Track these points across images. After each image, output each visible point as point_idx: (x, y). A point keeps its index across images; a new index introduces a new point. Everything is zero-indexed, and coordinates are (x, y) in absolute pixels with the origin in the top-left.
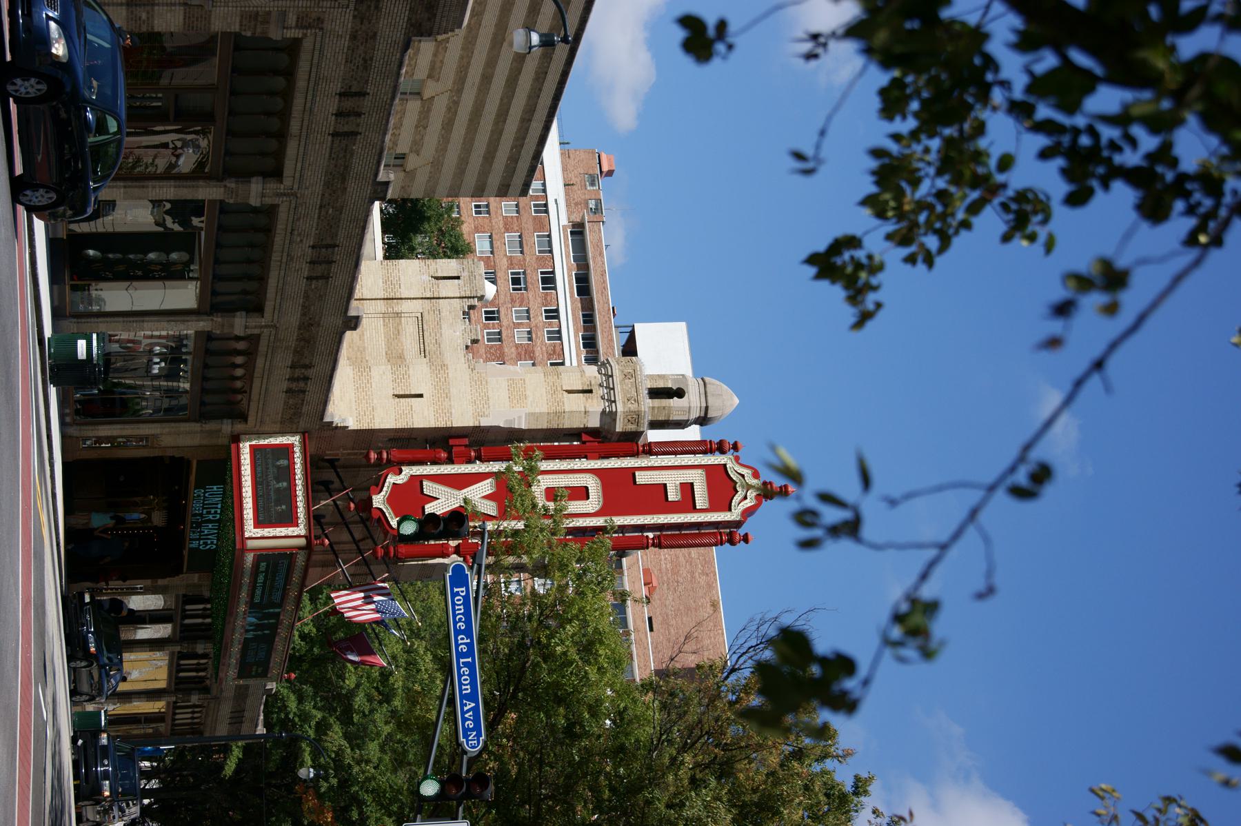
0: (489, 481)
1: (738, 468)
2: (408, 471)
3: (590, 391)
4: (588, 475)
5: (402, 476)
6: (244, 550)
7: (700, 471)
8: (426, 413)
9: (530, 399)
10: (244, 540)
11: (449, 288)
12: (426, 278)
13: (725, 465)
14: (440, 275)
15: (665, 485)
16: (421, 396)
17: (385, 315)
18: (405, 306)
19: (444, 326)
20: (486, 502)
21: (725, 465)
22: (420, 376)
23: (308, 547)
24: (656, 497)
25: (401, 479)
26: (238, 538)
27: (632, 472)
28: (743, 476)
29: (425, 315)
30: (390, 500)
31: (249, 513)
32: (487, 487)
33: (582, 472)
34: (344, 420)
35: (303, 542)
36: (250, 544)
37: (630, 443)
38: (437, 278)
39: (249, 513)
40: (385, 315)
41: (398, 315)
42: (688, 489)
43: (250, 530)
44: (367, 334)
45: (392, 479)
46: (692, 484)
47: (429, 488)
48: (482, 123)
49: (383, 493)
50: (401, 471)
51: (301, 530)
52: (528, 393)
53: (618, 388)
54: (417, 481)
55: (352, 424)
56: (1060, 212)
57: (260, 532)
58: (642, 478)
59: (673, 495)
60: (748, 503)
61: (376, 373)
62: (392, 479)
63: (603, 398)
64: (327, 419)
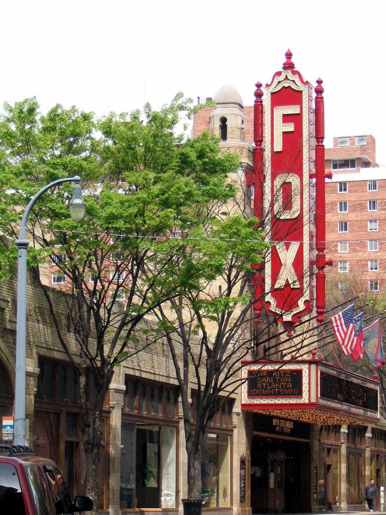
1: (273, 86)
7: (275, 110)
15: (284, 133)
24: (292, 140)
27: (275, 154)
32: (280, 247)
42: (287, 118)
50: (269, 303)
58: (278, 147)
59: (290, 127)
62: (273, 308)
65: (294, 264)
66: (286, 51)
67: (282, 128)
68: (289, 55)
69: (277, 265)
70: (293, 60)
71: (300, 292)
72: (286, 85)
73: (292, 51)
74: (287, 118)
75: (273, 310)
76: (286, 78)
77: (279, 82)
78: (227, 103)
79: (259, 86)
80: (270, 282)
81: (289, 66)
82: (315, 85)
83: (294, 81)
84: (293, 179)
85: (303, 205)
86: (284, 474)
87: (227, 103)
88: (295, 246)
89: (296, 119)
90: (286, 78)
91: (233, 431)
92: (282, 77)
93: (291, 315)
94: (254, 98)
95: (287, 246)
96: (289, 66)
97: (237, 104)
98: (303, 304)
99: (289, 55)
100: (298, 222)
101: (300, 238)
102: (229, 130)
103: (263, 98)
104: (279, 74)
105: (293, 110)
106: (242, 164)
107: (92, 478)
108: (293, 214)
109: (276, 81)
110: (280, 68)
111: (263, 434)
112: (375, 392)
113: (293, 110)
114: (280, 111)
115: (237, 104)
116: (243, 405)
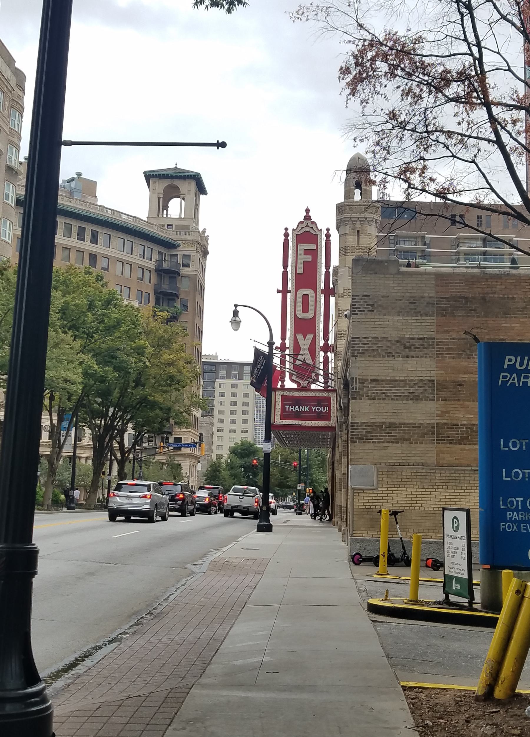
42: (307, 252)
58: (300, 271)
59: (309, 258)
65: (309, 349)
67: (303, 258)
68: (307, 211)
70: (310, 214)
73: (309, 208)
74: (307, 252)
76: (307, 226)
77: (302, 228)
79: (286, 229)
81: (307, 218)
82: (326, 232)
83: (312, 228)
84: (310, 292)
86: (464, 270)
89: (314, 253)
90: (307, 226)
92: (305, 224)
94: (284, 238)
96: (307, 218)
99: (307, 211)
100: (313, 321)
103: (289, 238)
105: (312, 247)
108: (301, 292)
111: (18, 719)
112: (255, 490)
113: (312, 247)
114: (302, 247)
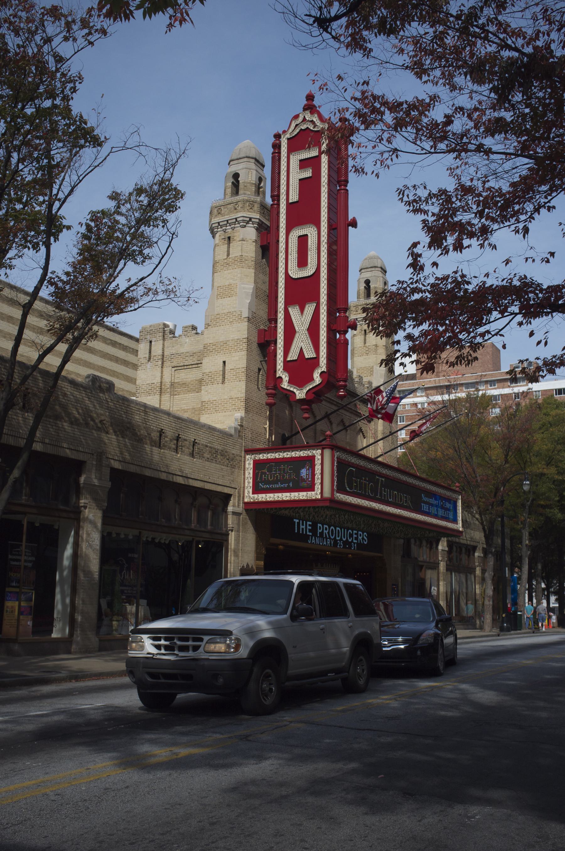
0: (290, 309)
1: (290, 130)
2: (280, 372)
3: (229, 238)
4: (290, 236)
5: (283, 377)
6: (332, 500)
7: (291, 156)
8: (237, 358)
9: (231, 281)
10: (323, 499)
11: (157, 349)
12: (149, 365)
13: (288, 139)
14: (147, 356)
15: (300, 180)
16: (224, 362)
17: (172, 394)
18: (167, 379)
19: (182, 350)
20: (305, 312)
21: (288, 139)
22: (212, 364)
23: (334, 448)
24: (309, 187)
25: (285, 377)
26: (321, 504)
27: (289, 205)
28: (297, 125)
29: (173, 365)
30: (300, 385)
31: (302, 495)
32: (294, 312)
33: (287, 242)
34: (236, 420)
35: (327, 453)
36: (327, 494)
37: (271, 212)
38: (150, 358)
39: (302, 495)
40: (172, 394)
41: (172, 384)
42: (303, 164)
43: (315, 495)
44: (185, 407)
45: (285, 385)
46: (301, 161)
47: (293, 355)
48: (91, 361)
49: (295, 391)
50: (280, 378)
51: (317, 453)
52: (227, 283)
53: (227, 218)
54: (288, 365)
55: (240, 414)
56: (402, 351)
57: (318, 487)
58: (294, 197)
59: (308, 173)
60: (315, 119)
61: (205, 398)
62: (285, 385)
63: (233, 229)
64: (232, 432)
66: (307, 92)
69: (313, 330)
71: (315, 362)
72: (304, 127)
75: (285, 387)
78: (240, 159)
80: (282, 354)
85: (318, 260)
87: (240, 159)
88: (310, 309)
90: (304, 119)
91: (228, 535)
92: (301, 119)
93: (305, 391)
95: (302, 310)
97: (252, 158)
98: (318, 375)
101: (316, 299)
102: (241, 186)
104: (296, 117)
106: (221, 224)
107: (477, 411)
109: (293, 125)
110: (299, 109)
114: (295, 159)
115: (252, 158)
116: (246, 503)
